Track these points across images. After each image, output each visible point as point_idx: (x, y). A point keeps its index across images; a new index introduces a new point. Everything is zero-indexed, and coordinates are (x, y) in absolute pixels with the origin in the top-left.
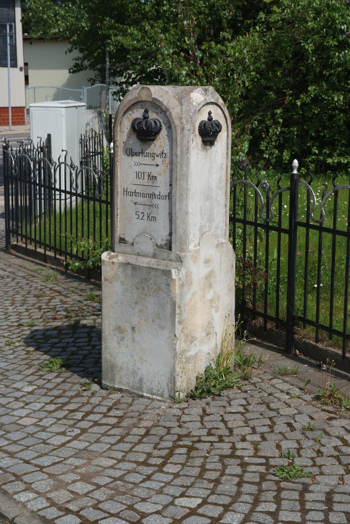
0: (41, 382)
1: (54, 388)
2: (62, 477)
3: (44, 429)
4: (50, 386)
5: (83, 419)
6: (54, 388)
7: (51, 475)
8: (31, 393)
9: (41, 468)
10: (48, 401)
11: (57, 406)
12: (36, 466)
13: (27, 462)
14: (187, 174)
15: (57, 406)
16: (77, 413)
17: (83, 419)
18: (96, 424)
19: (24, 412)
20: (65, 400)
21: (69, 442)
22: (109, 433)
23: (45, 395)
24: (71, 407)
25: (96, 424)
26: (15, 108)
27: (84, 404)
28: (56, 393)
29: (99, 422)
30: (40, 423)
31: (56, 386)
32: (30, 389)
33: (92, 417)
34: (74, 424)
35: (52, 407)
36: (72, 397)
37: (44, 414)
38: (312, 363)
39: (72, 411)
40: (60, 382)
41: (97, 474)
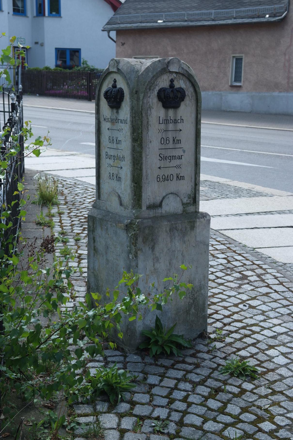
0: (261, 357)
1: (249, 345)
2: (258, 279)
3: (263, 313)
4: (254, 350)
5: (234, 313)
6: (249, 345)
7: (263, 281)
8: (271, 347)
9: (268, 286)
10: (256, 334)
11: (250, 328)
12: (271, 288)
13: (276, 291)
14: (142, 137)
15: (250, 328)
16: (236, 318)
17: (234, 313)
18: (226, 308)
19: (278, 329)
20: (242, 331)
21: (248, 300)
22: (220, 300)
23: (259, 341)
24: (239, 325)
25: (226, 308)
26: (117, 53)
27: (229, 324)
28: (248, 340)
29: (223, 308)
30: (266, 318)
31: (246, 347)
32: (271, 352)
33: (227, 313)
34: (240, 311)
35: (254, 328)
36: (236, 332)
37: (262, 324)
38: (17, 359)
39: (240, 321)
40: (243, 351)
41: (238, 279)
